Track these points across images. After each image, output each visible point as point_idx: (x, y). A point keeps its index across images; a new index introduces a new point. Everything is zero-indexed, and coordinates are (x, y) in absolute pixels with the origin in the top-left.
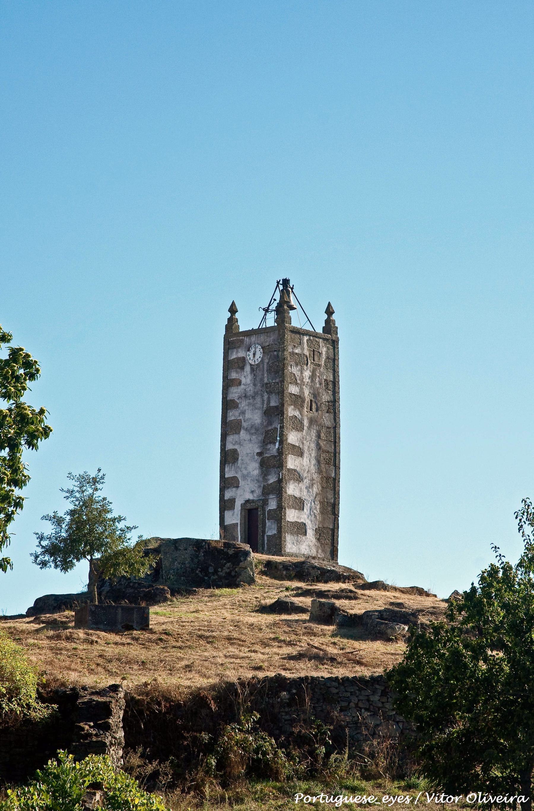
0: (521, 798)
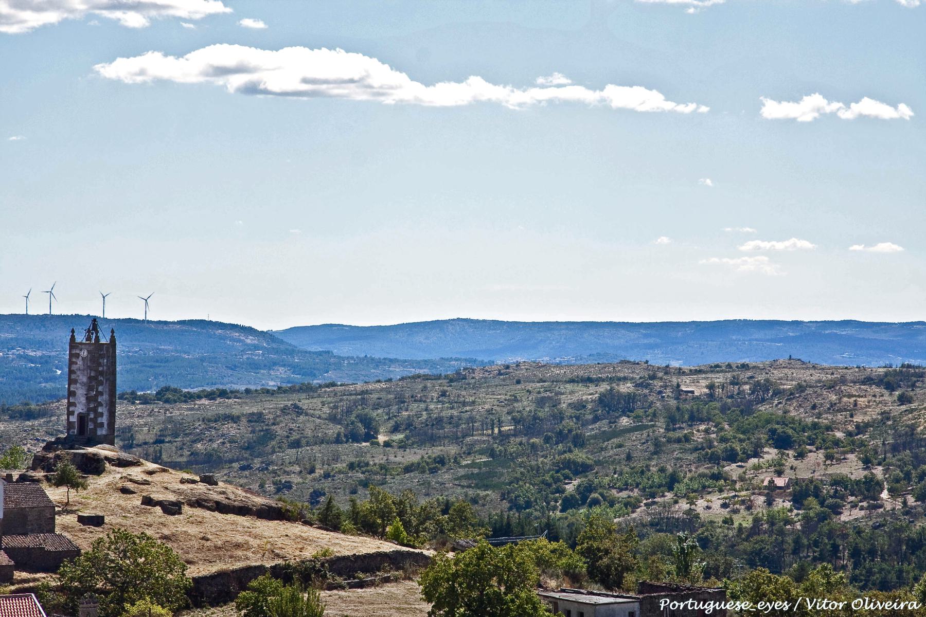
0: (912, 605)
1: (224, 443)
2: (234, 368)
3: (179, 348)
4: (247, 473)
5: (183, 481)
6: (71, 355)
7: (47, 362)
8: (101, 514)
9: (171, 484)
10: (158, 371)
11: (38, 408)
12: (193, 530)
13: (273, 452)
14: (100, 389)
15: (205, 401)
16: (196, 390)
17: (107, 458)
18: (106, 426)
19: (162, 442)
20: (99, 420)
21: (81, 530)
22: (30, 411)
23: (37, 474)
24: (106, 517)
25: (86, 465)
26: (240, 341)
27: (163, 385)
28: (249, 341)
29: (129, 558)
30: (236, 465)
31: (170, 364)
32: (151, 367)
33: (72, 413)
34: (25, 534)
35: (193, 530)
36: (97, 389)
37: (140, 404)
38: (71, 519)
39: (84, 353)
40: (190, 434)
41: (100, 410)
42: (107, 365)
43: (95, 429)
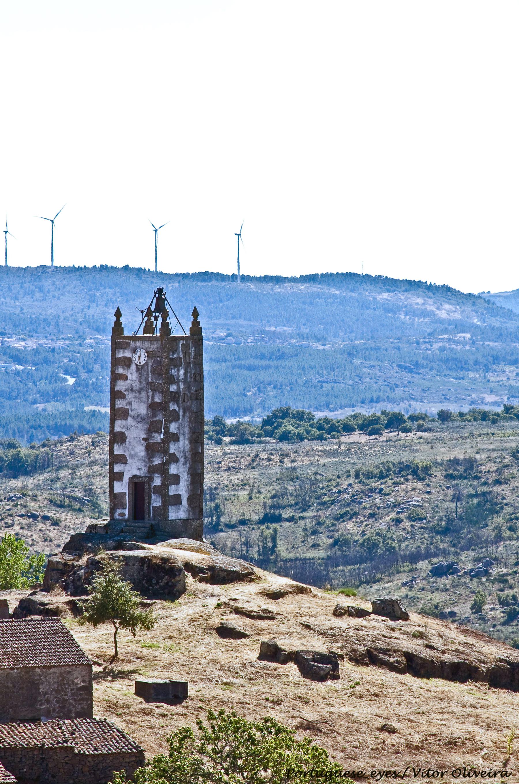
1: (398, 521)
2: (414, 368)
3: (305, 330)
4: (445, 581)
5: (338, 613)
6: (115, 362)
7: (47, 361)
8: (180, 679)
9: (312, 617)
10: (264, 376)
11: (33, 452)
12: (363, 711)
13: (499, 538)
14: (173, 428)
15: (358, 437)
16: (340, 415)
17: (189, 567)
18: (185, 501)
19: (278, 519)
20: (172, 491)
21: (144, 712)
22: (17, 459)
23: (54, 599)
24: (190, 686)
25: (149, 581)
26: (425, 314)
27: (275, 405)
28: (443, 314)
29: (242, 769)
30: (424, 566)
31: (288, 363)
32: (250, 368)
33: (119, 477)
34: (35, 720)
35: (363, 711)
36: (167, 428)
37: (232, 443)
38: (122, 690)
39: (141, 357)
40: (333, 502)
41: (173, 469)
42: (185, 381)
43: (163, 510)
